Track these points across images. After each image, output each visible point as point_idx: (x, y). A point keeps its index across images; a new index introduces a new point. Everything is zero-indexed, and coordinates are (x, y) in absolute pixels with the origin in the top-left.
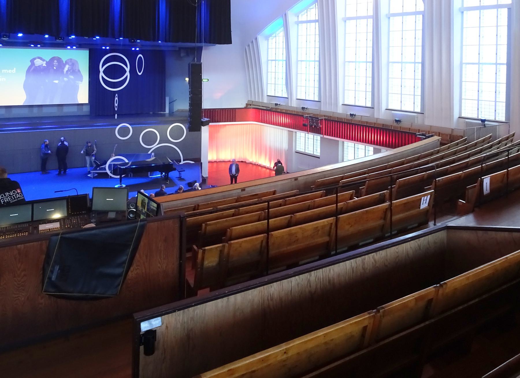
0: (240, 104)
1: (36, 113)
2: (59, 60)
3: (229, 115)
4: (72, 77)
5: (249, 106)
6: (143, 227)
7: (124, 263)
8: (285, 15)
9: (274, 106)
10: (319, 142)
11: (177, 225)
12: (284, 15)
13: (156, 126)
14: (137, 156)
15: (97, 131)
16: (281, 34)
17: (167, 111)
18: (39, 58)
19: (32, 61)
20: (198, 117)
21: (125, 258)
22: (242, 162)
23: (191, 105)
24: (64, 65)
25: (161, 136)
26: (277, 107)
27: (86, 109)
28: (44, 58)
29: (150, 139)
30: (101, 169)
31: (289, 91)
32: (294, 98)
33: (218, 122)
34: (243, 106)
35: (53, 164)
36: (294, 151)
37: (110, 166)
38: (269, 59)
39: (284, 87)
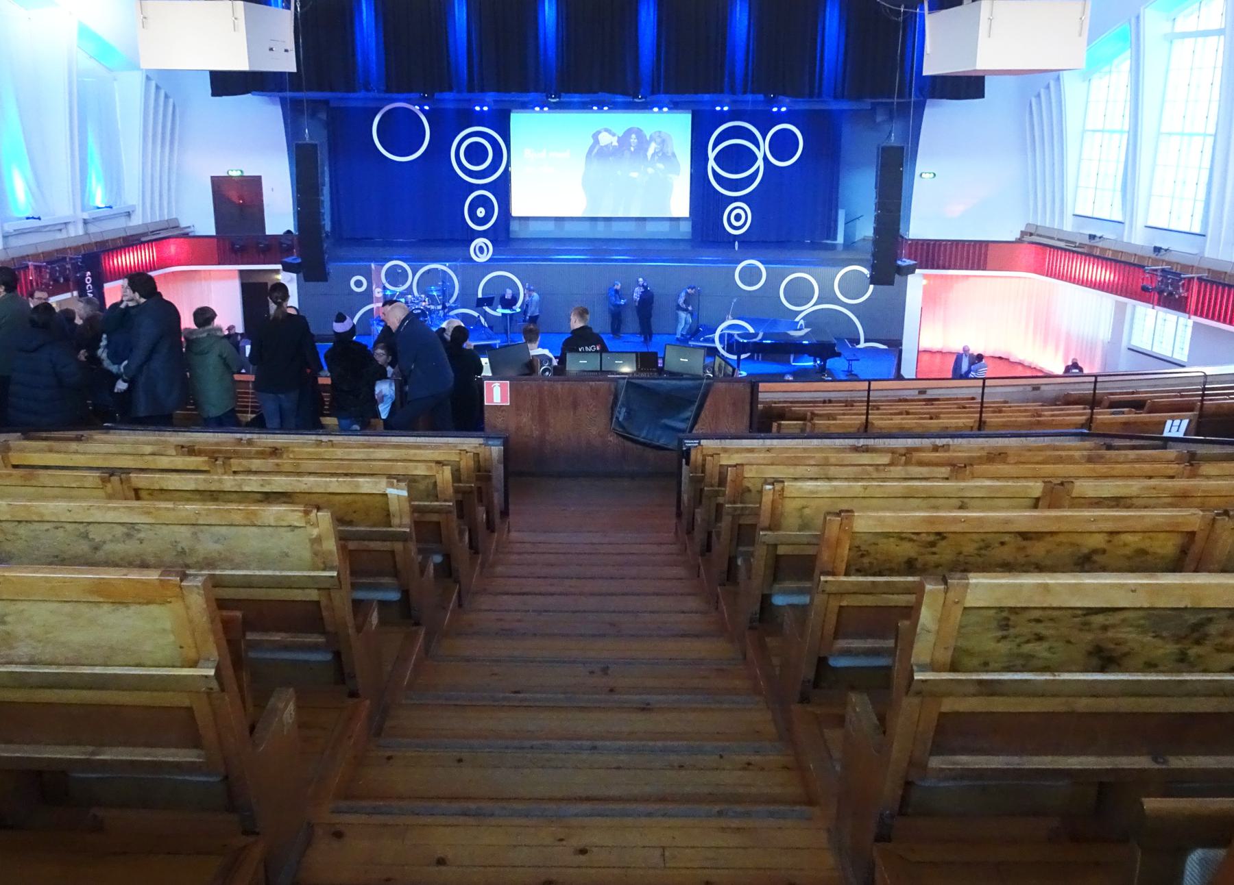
0: (1006, 230)
1: (601, 231)
2: (639, 133)
3: (971, 255)
4: (660, 166)
5: (1027, 238)
6: (709, 386)
7: (688, 419)
8: (1138, 18)
9: (1086, 241)
10: (1189, 330)
11: (748, 390)
12: (1133, 21)
13: (812, 268)
14: (775, 322)
15: (703, 269)
16: (1124, 65)
17: (840, 239)
18: (606, 130)
19: (595, 136)
20: (892, 256)
21: (689, 414)
22: (1000, 358)
23: (876, 231)
24: (648, 143)
25: (823, 290)
26: (1093, 243)
27: (686, 228)
28: (614, 130)
29: (799, 293)
30: (706, 340)
31: (1129, 208)
32: (1140, 223)
33: (944, 268)
34: (1013, 236)
35: (631, 322)
36: (1124, 344)
37: (721, 336)
38: (1088, 127)
39: (1119, 195)
